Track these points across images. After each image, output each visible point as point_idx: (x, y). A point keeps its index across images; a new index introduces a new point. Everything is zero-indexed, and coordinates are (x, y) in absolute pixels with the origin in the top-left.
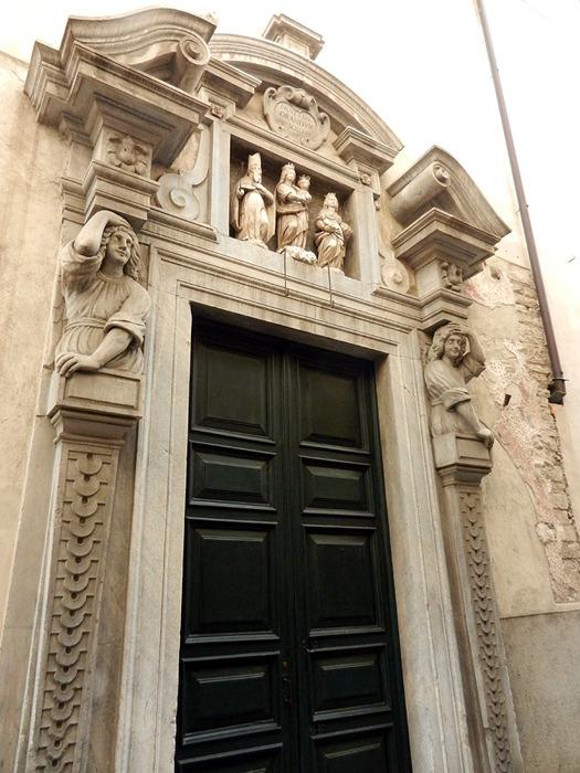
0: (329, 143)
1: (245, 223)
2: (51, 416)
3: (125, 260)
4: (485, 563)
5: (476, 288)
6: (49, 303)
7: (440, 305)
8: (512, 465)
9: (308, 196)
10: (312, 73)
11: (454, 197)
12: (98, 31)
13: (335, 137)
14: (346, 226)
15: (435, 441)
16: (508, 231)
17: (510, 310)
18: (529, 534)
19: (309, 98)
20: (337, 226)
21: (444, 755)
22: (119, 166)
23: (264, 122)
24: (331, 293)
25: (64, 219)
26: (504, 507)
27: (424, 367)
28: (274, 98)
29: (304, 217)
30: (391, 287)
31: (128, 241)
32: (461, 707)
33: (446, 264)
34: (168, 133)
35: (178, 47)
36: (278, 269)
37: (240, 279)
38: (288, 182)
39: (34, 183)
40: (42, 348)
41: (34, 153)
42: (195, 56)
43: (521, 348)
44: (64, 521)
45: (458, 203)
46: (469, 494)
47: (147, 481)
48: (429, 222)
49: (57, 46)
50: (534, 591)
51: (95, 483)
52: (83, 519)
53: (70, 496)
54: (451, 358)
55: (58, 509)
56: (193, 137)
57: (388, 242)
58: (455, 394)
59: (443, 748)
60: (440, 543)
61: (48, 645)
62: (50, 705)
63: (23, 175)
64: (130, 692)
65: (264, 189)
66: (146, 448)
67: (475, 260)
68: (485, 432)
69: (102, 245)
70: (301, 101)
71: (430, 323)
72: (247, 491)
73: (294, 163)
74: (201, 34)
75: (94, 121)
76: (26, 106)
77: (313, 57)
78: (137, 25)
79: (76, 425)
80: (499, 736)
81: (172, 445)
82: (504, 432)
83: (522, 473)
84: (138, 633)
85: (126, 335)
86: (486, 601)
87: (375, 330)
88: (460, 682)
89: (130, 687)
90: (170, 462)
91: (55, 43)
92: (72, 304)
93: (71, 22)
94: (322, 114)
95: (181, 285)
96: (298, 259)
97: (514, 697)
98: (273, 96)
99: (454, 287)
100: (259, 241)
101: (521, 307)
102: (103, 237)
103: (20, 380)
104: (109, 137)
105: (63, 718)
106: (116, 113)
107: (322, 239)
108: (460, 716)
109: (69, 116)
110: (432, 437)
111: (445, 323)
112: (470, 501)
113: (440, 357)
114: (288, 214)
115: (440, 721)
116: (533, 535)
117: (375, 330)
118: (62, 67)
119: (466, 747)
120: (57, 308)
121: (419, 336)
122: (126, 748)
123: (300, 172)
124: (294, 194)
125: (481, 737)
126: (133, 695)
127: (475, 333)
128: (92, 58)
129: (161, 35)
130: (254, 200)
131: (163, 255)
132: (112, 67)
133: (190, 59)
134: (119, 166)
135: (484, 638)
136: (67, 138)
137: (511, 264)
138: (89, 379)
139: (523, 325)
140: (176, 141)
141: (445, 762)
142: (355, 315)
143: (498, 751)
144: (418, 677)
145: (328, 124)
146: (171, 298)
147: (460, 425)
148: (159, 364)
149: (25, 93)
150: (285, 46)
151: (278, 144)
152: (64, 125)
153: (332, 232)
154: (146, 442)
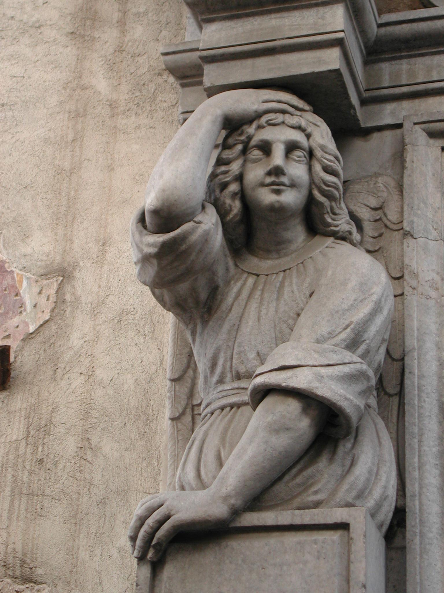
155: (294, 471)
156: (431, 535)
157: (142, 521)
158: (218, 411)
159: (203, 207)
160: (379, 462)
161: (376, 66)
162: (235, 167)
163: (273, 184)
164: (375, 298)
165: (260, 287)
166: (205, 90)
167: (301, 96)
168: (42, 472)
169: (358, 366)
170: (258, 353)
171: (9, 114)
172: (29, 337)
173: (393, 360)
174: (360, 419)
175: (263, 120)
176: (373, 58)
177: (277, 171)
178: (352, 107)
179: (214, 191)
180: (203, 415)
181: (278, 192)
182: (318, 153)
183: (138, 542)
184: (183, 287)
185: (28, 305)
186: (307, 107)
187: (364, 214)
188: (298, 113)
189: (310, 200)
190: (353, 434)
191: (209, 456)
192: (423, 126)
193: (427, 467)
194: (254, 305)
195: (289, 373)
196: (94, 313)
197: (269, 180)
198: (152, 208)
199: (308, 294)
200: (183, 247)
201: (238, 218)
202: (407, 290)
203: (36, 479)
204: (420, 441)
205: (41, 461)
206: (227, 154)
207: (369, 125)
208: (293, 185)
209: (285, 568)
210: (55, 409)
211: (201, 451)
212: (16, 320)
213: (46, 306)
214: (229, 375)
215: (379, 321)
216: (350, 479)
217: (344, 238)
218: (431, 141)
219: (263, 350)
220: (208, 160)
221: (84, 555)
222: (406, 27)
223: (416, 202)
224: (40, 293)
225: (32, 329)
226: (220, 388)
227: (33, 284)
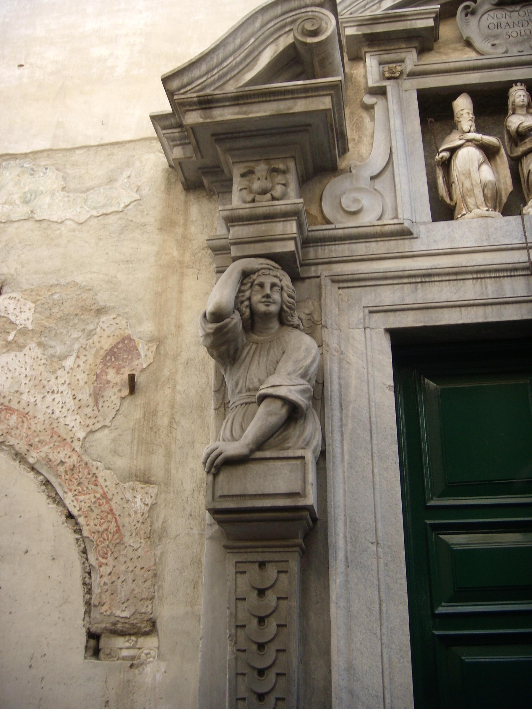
12: (196, 72)
22: (253, 201)
23: (468, 49)
31: (273, 285)
37: (456, 274)
38: (519, 111)
42: (315, 33)
44: (238, 650)
51: (271, 598)
52: (261, 646)
53: (243, 616)
63: (176, 253)
66: (341, 543)
73: (521, 81)
76: (173, 180)
78: (238, 42)
81: (380, 534)
85: (279, 403)
90: (378, 558)
91: (166, 108)
93: (166, 80)
106: (240, 143)
120: (217, 391)
128: (194, 103)
129: (272, 34)
131: (338, 281)
132: (218, 101)
133: (310, 40)
134: (253, 201)
138: (240, 470)
146: (358, 334)
148: (350, 426)
154: (341, 535)
155: (278, 433)
156: (337, 462)
157: (209, 455)
158: (239, 406)
159: (234, 312)
160: (315, 430)
161: (307, 249)
162: (247, 294)
163: (265, 302)
164: (313, 355)
165: (259, 349)
166: (232, 258)
167: (276, 262)
168: (152, 433)
169: (307, 386)
170: (259, 379)
171: (131, 265)
172: (143, 370)
173: (318, 383)
174: (307, 410)
175: (260, 272)
176: (305, 245)
177: (268, 296)
178: (297, 267)
179: (238, 304)
180: (231, 408)
181: (267, 305)
182: (285, 288)
183: (207, 465)
184: (223, 348)
185: (143, 354)
186: (280, 267)
187: (303, 316)
188: (276, 270)
189: (281, 310)
190: (304, 417)
191: (237, 426)
192: (330, 277)
193: (335, 432)
194: (256, 358)
195: (276, 388)
196: (175, 359)
197: (263, 300)
198: (211, 311)
199: (282, 353)
200: (226, 330)
201: (248, 317)
202: (325, 352)
203: (149, 436)
204: (332, 420)
205: (152, 428)
206: (243, 288)
207: (304, 276)
208: (274, 303)
209: (276, 476)
210: (158, 404)
211: (232, 424)
212: (136, 362)
213: (151, 355)
214: (244, 390)
215: (315, 365)
216: (304, 436)
217: (297, 327)
218: (333, 284)
219: (262, 378)
220: (236, 290)
221: (173, 471)
222: (321, 232)
223: (327, 312)
224: (148, 349)
225: (144, 366)
226: (240, 395)
227: (145, 345)
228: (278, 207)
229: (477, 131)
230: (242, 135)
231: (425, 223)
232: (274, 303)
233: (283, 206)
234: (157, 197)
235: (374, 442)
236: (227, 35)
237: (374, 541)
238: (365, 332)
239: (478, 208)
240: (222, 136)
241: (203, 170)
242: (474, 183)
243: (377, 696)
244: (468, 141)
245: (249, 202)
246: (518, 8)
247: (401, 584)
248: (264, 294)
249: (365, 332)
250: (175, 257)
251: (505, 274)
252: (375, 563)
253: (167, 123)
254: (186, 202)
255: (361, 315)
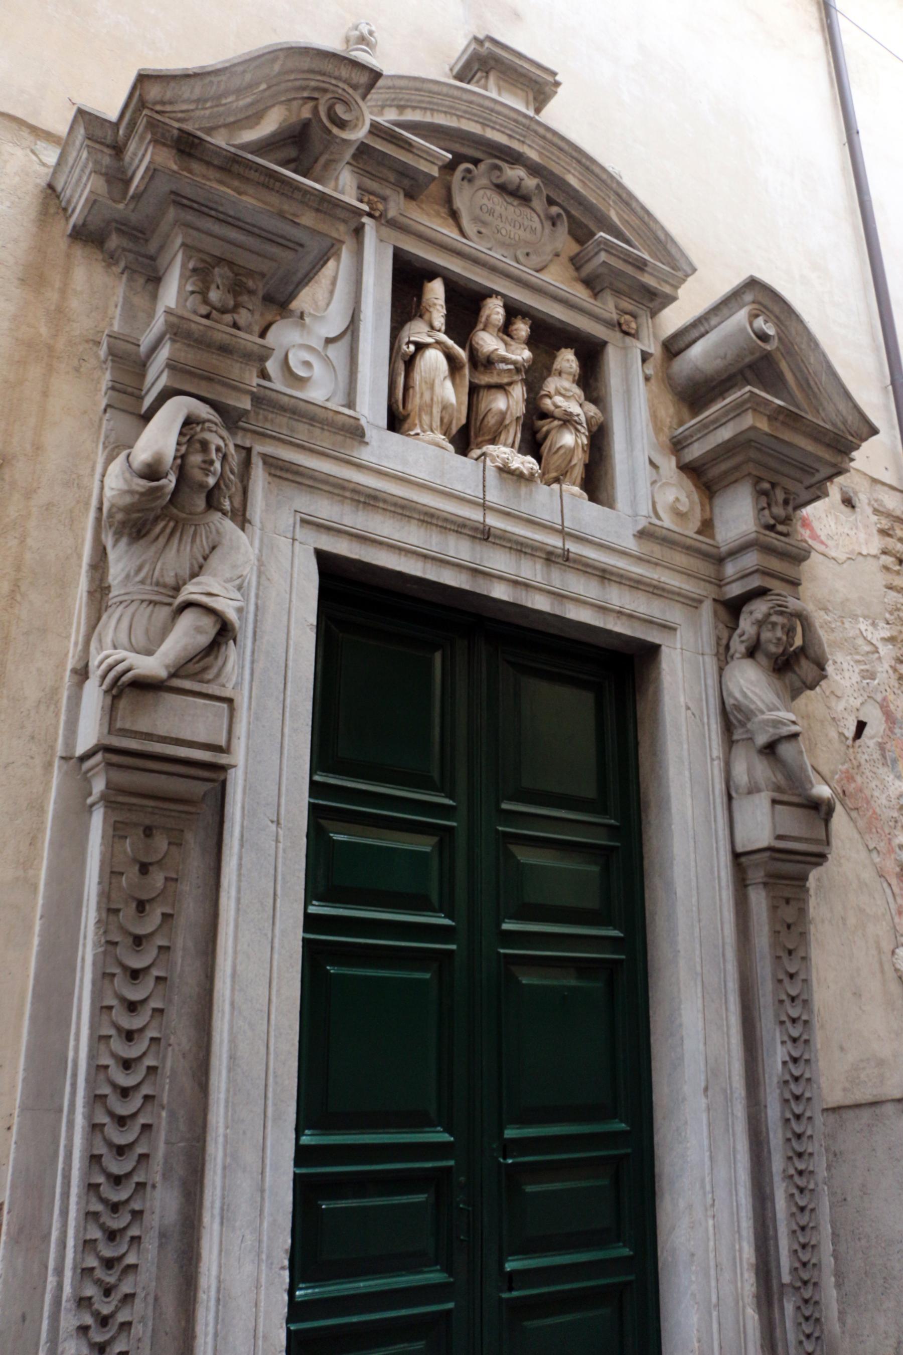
0: (564, 259)
1: (415, 402)
2: (84, 758)
3: (211, 481)
4: (804, 1017)
5: (815, 524)
6: (80, 557)
7: (751, 560)
8: (861, 847)
9: (527, 354)
10: (537, 139)
11: (784, 366)
13: (574, 248)
14: (592, 409)
15: (735, 803)
16: (874, 431)
17: (872, 566)
18: (881, 964)
19: (531, 183)
20: (575, 408)
21: (715, 1326)
24: (562, 533)
25: (108, 406)
26: (844, 919)
27: (721, 670)
28: (470, 181)
29: (518, 392)
30: (667, 521)
31: (218, 449)
32: (748, 1252)
33: (766, 486)
34: (288, 255)
35: (315, 110)
36: (472, 490)
38: (490, 329)
39: (61, 344)
40: (68, 637)
41: (63, 291)
42: (342, 124)
43: (887, 634)
45: (789, 377)
46: (788, 901)
47: (239, 875)
48: (738, 410)
49: (113, 114)
50: (881, 1063)
54: (768, 655)
55: (99, 922)
56: (331, 264)
57: (665, 439)
58: (777, 723)
59: (715, 1314)
60: (733, 986)
61: (89, 1142)
62: (95, 1233)
63: (44, 330)
64: (217, 1220)
65: (450, 342)
67: (818, 477)
68: (823, 791)
69: (175, 458)
70: (519, 187)
71: (735, 590)
72: (724, 324)
73: (504, 296)
74: (355, 87)
75: (168, 236)
76: (52, 210)
77: (538, 111)
79: (124, 778)
80: (807, 1296)
82: (851, 788)
83: (877, 860)
84: (227, 1127)
86: (803, 1082)
87: (640, 604)
88: (751, 1214)
89: (217, 1211)
92: (118, 560)
94: (555, 210)
95: (303, 521)
96: (505, 470)
97: (835, 1235)
98: (468, 178)
99: (780, 528)
100: (440, 437)
101: (889, 560)
102: (179, 444)
103: (32, 693)
104: (191, 265)
105: (116, 1254)
107: (548, 433)
108: (745, 1266)
109: (126, 229)
110: (730, 798)
111: (761, 593)
112: (788, 913)
113: (751, 653)
114: (490, 387)
115: (713, 1272)
116: (887, 967)
117: (640, 604)
118: (118, 150)
119: (752, 1316)
121: (715, 613)
122: (212, 1303)
123: (513, 311)
124: (502, 351)
125: (776, 1297)
126: (222, 1223)
127: (810, 608)
130: (434, 360)
134: (207, 316)
135: (794, 1143)
136: (116, 263)
137: (875, 481)
139: (892, 594)
140: (304, 267)
141: (716, 1336)
142: (604, 575)
143: (802, 1320)
144: (682, 1204)
145: (563, 228)
146: (284, 543)
147: (781, 779)
149: (50, 186)
150: (493, 94)
151: (476, 261)
152: (114, 241)
153: (568, 421)
196: (28, 495)
208: (214, 474)
214: (149, 581)
228: (242, 341)
229: (446, 333)
230: (213, 213)
231: (378, 427)
232: (214, 474)
233: (249, 344)
234: (22, 225)
235: (288, 692)
236: (240, 60)
237: (275, 819)
238: (293, 545)
239: (432, 431)
240: (185, 202)
241: (119, 226)
242: (435, 399)
243: (261, 1011)
244: (438, 342)
245: (202, 316)
246: (515, 203)
247: (298, 877)
248: (207, 458)
249: (293, 545)
250: (41, 335)
251: (452, 528)
252: (274, 846)
253: (99, 133)
254: (68, 256)
255: (291, 521)
